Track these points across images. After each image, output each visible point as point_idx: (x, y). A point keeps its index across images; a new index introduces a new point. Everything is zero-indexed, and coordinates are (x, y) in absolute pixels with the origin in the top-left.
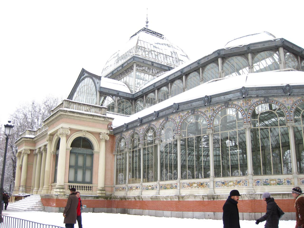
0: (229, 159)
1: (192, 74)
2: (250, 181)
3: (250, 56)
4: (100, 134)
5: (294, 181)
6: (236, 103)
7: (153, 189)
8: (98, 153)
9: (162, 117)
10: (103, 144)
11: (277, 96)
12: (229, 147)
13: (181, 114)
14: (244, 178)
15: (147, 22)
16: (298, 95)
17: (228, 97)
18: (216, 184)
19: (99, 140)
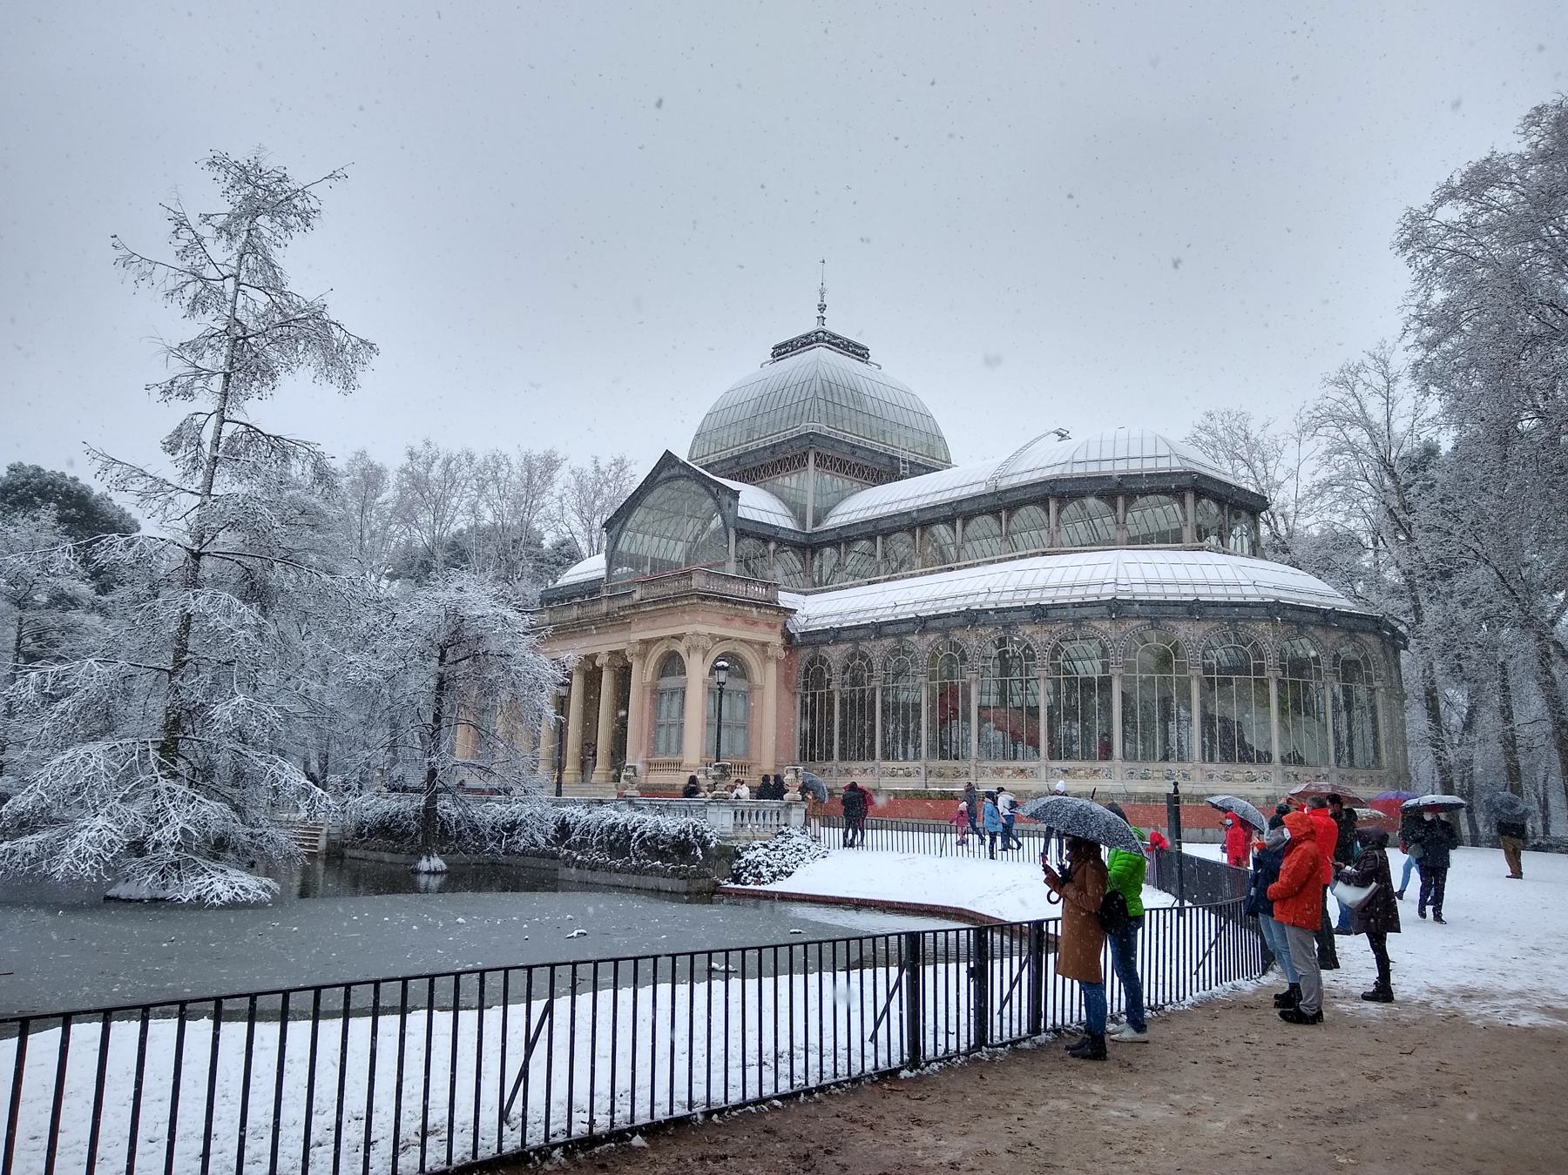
0: (1051, 729)
1: (979, 519)
2: (1118, 770)
3: (1120, 501)
4: (765, 645)
5: (1362, 409)
6: (1096, 624)
7: (908, 775)
8: (762, 688)
9: (935, 630)
10: (772, 669)
11: (1175, 619)
12: (1276, 757)
13: (981, 631)
14: (1104, 765)
15: (822, 308)
16: (1213, 620)
17: (1086, 611)
18: (1052, 774)
19: (766, 659)
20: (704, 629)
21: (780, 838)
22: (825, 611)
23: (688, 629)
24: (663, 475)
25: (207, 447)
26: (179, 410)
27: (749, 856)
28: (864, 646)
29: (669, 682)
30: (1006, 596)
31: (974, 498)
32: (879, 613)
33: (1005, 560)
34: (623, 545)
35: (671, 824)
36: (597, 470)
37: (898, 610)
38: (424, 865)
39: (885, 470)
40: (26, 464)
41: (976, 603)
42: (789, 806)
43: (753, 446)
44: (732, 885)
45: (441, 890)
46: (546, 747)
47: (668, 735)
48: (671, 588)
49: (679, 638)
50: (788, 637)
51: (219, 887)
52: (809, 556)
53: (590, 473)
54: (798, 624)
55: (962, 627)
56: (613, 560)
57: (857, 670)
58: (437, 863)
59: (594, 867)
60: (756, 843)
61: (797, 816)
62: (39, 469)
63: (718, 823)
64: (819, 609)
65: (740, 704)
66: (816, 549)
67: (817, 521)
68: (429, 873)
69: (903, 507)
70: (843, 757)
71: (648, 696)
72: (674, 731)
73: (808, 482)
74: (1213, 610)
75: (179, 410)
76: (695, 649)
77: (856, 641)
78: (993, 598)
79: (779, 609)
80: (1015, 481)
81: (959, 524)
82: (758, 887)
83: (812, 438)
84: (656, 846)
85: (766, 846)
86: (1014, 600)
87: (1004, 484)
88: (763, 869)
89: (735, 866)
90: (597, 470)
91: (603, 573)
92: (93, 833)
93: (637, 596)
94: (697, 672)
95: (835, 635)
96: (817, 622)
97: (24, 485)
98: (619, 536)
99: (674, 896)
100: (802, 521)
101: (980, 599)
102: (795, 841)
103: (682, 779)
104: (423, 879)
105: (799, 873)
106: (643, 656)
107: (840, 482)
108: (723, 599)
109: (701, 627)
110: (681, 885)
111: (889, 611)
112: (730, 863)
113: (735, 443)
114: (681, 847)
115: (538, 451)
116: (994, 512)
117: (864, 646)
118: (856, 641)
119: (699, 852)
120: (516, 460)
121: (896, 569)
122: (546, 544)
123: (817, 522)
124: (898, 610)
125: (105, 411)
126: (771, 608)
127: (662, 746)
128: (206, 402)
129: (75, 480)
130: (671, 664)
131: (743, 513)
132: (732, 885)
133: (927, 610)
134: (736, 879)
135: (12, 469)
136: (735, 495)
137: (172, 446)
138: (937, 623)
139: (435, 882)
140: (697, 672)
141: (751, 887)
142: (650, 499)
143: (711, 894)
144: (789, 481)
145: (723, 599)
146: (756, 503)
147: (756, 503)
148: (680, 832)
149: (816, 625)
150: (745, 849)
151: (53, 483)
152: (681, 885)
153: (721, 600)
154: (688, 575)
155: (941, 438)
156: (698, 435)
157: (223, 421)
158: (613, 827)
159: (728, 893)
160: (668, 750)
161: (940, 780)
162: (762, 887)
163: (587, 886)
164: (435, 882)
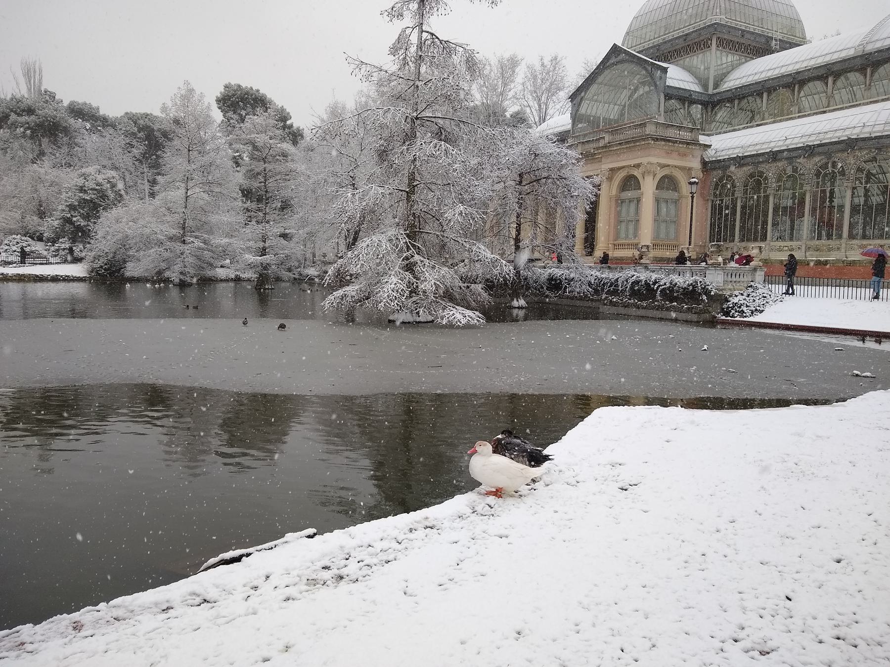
4: (690, 169)
9: (819, 154)
13: (858, 153)
20: (654, 160)
21: (750, 290)
22: (729, 146)
23: (644, 160)
24: (611, 61)
25: (413, 49)
26: (398, 26)
27: (736, 300)
28: (762, 168)
29: (629, 194)
30: (877, 128)
31: (844, 61)
32: (772, 145)
33: (847, 108)
34: (583, 110)
35: (682, 279)
36: (543, 65)
37: (788, 142)
38: (515, 303)
39: (761, 47)
40: (233, 83)
41: (854, 134)
42: (755, 270)
43: (669, 37)
44: (724, 318)
45: (526, 318)
46: (580, 233)
47: (627, 230)
48: (630, 134)
49: (638, 166)
50: (704, 164)
51: (459, 316)
52: (709, 109)
53: (538, 67)
54: (710, 155)
55: (843, 151)
56: (576, 118)
57: (757, 182)
58: (522, 302)
59: (626, 306)
60: (736, 293)
61: (760, 276)
62: (239, 86)
63: (714, 280)
64: (728, 142)
65: (672, 207)
66: (751, 102)
67: (716, 86)
68: (518, 308)
69: (783, 71)
70: (742, 240)
71: (613, 203)
72: (631, 227)
73: (714, 59)
74: (861, 144)
75: (398, 26)
76: (649, 172)
77: (756, 164)
78: (867, 130)
79: (700, 145)
80: (878, 45)
81: (830, 80)
82: (742, 319)
83: (715, 27)
84: (670, 293)
85: (742, 294)
86: (884, 131)
87: (870, 48)
88: (745, 309)
89: (725, 306)
90: (543, 65)
91: (569, 127)
92: (393, 286)
93: (607, 140)
94: (649, 187)
95: (740, 161)
96: (723, 153)
97: (234, 95)
98: (580, 104)
99: (697, 323)
100: (705, 86)
101: (857, 131)
102: (760, 291)
103: (675, 254)
104: (515, 312)
105: (767, 309)
106: (610, 179)
107: (729, 58)
108: (665, 140)
109: (654, 159)
110: (694, 317)
111: (781, 143)
112: (722, 304)
113: (653, 37)
114: (691, 294)
115: (507, 55)
116: (862, 70)
117: (762, 168)
118: (756, 164)
119: (705, 297)
120: (494, 61)
121: (753, 119)
122: (508, 115)
123: (716, 86)
124: (788, 142)
125: (3, 97)
126: (695, 144)
127: (623, 235)
128: (408, 20)
129: (258, 91)
130: (630, 182)
131: (669, 82)
132: (724, 318)
133: (814, 141)
134: (727, 314)
135: (226, 87)
136: (665, 70)
137: (394, 50)
138: (821, 149)
139: (521, 313)
140: (649, 187)
141: (738, 319)
142: (600, 79)
143: (712, 323)
144: (697, 60)
145: (665, 140)
146: (677, 76)
147: (677, 76)
148: (689, 285)
149: (723, 155)
150: (731, 296)
151: (247, 93)
152: (694, 317)
153: (664, 140)
154: (643, 125)
155: (800, 21)
156: (627, 33)
157: (422, 31)
158: (637, 282)
159: (723, 323)
160: (627, 237)
161: (818, 253)
162: (745, 319)
163: (618, 317)
164: (521, 313)
